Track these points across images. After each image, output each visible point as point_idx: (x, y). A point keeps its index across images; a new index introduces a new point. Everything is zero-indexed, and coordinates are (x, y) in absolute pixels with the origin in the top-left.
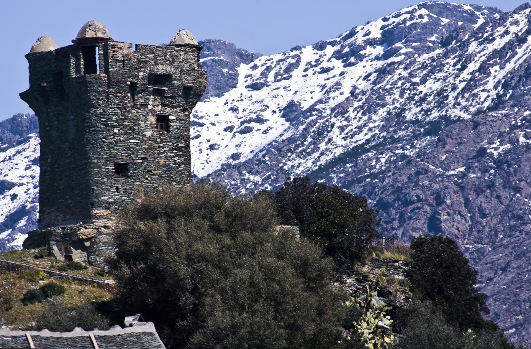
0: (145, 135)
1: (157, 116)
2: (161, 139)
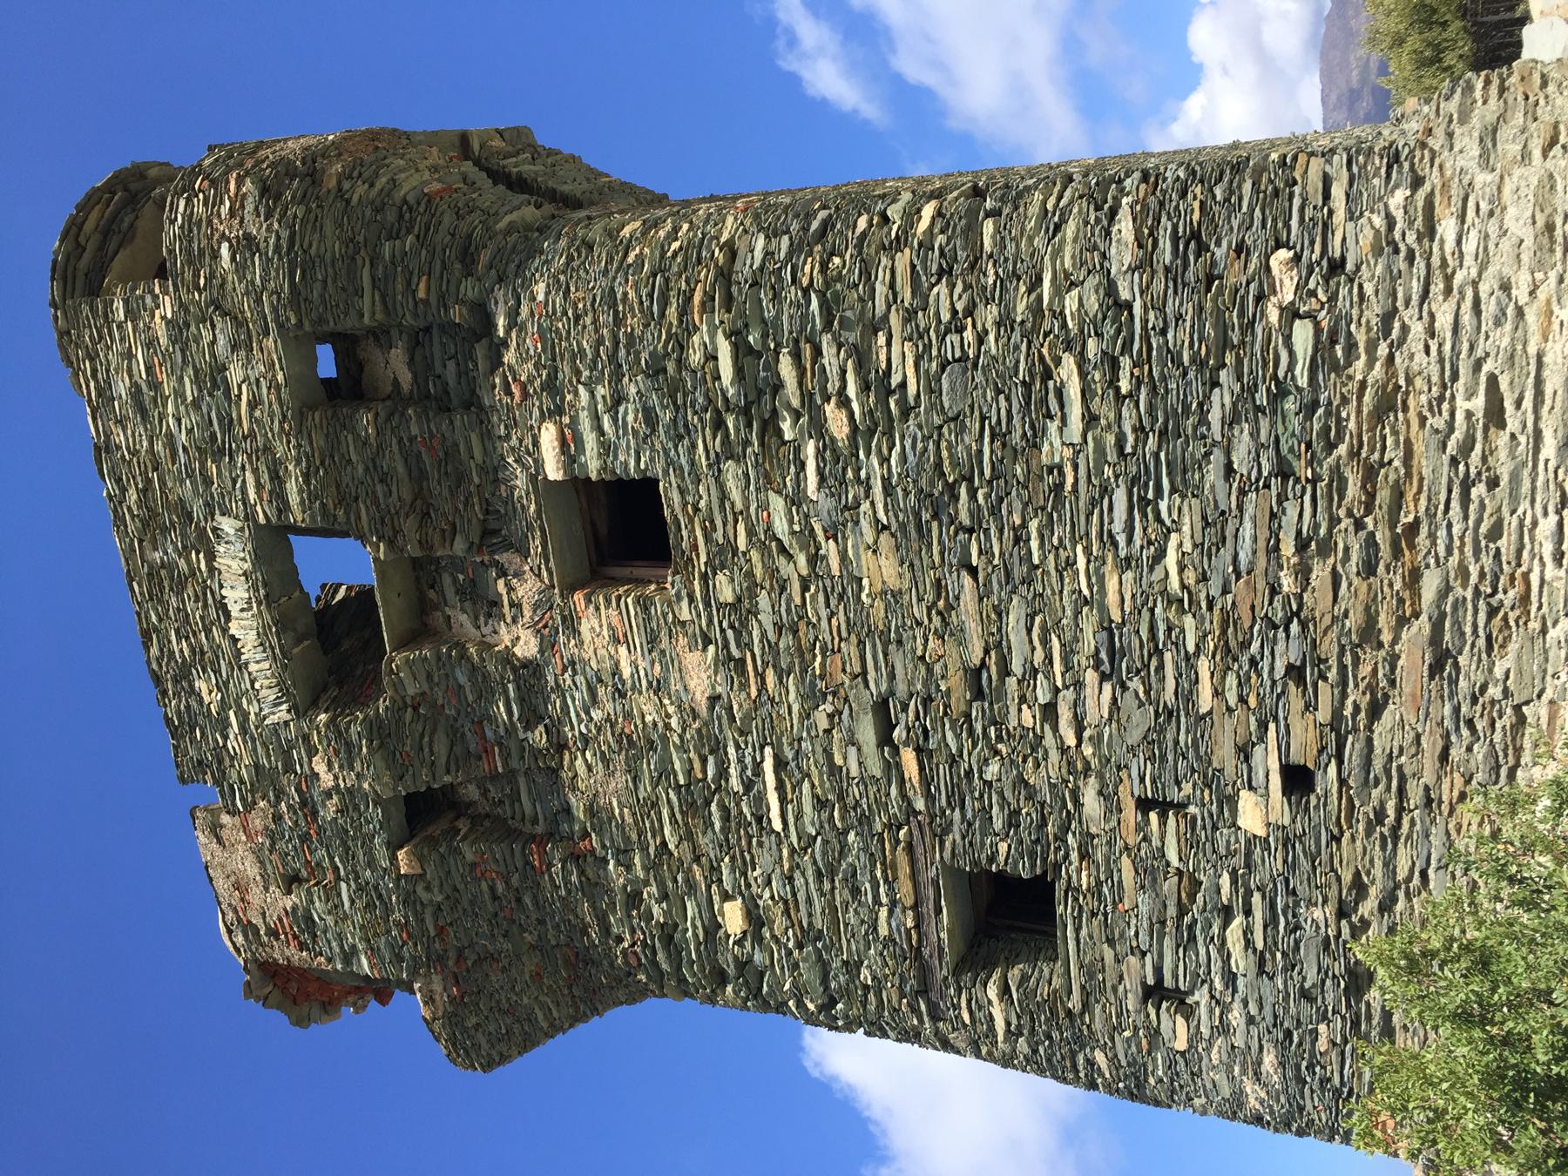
0: (714, 699)
1: (569, 589)
2: (714, 567)
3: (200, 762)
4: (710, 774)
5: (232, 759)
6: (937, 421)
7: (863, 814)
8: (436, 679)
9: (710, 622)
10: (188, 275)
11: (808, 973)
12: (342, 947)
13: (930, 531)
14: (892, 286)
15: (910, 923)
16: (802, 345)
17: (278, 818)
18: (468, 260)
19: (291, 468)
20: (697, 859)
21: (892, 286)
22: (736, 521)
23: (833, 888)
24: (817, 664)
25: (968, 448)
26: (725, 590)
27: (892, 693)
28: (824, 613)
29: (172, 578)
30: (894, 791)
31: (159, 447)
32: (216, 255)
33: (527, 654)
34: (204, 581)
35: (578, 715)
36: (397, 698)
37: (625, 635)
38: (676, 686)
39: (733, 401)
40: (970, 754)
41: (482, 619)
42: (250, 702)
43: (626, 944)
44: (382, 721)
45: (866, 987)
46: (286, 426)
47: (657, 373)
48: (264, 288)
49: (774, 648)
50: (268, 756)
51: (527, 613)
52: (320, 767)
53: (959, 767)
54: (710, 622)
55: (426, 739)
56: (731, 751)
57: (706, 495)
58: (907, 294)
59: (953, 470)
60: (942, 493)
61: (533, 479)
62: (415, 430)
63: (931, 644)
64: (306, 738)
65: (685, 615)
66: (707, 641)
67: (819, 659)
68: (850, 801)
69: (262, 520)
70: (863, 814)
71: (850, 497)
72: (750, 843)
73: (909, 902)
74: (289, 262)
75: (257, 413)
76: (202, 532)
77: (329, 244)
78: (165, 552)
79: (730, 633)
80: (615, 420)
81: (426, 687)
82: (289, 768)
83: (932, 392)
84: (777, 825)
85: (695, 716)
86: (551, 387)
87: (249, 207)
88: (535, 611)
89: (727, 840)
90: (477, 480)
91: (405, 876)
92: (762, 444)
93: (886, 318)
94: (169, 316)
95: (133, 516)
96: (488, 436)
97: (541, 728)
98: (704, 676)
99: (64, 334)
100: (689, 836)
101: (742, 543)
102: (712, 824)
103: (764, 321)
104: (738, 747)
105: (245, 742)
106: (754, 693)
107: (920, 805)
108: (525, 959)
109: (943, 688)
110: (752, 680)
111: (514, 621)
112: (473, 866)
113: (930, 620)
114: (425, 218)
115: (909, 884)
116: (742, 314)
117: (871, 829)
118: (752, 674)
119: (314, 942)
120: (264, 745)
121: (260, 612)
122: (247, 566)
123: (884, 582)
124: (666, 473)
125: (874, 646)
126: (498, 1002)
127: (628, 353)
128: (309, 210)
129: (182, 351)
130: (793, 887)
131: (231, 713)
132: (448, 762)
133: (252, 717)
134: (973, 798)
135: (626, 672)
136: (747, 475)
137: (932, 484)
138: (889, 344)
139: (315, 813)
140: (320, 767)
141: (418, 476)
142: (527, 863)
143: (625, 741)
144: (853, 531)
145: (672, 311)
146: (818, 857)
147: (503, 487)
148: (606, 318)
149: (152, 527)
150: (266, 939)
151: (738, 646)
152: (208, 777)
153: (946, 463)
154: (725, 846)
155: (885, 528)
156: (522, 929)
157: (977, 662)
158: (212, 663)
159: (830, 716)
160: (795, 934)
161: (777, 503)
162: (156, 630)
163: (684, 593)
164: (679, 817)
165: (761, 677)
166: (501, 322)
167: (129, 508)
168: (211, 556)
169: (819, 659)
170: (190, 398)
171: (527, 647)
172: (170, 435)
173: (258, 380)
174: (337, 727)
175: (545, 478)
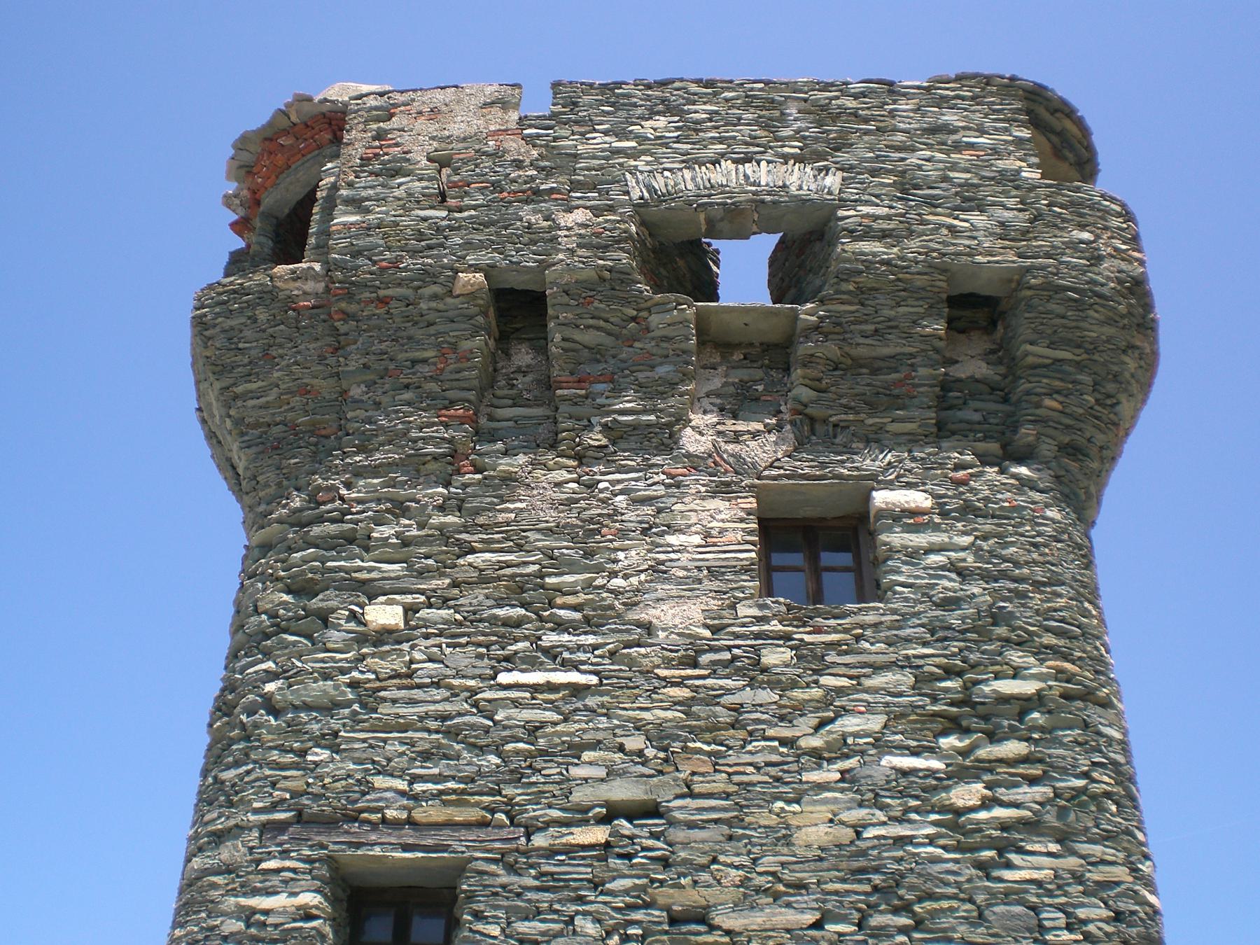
0: (648, 628)
3: (575, 104)
4: (562, 612)
5: (583, 134)
6: (980, 898)
7: (523, 775)
8: (664, 345)
9: (737, 636)
10: (1060, 199)
11: (318, 689)
12: (368, 199)
13: (860, 881)
14: (1103, 862)
15: (390, 813)
16: (1039, 766)
17: (518, 164)
18: (1070, 450)
19: (895, 250)
20: (455, 584)
21: (1103, 862)
22: (851, 677)
23: (429, 731)
24: (699, 745)
25: (954, 930)
26: (775, 657)
27: (672, 823)
28: (759, 759)
29: (771, 119)
30: (555, 813)
31: (900, 137)
32: (1082, 227)
33: (684, 441)
34: (771, 148)
35: (619, 482)
36: (649, 304)
37: (715, 545)
38: (662, 589)
39: (976, 689)
40: (605, 903)
41: (718, 401)
42: (648, 163)
43: (343, 492)
44: (628, 285)
45: (303, 753)
46: (935, 254)
47: (993, 616)
48: (1061, 263)
49: (713, 701)
50: (589, 169)
51: (730, 447)
52: (580, 216)
53: (589, 889)
54: (737, 636)
55: (602, 323)
56: (591, 639)
57: (874, 649)
58: (1095, 875)
59: (928, 912)
60: (901, 898)
61: (873, 477)
62: (922, 371)
63: (733, 872)
64: (611, 209)
65: (745, 611)
66: (715, 630)
67: (706, 748)
68: (539, 763)
69: (841, 213)
70: (523, 775)
71: (888, 800)
72: (479, 645)
73: (418, 815)
74: (1084, 290)
75: (945, 231)
76: (821, 156)
77: (1095, 328)
78: (795, 119)
79: (727, 656)
80: (943, 568)
81: (657, 333)
82: (576, 185)
83: (1006, 895)
84: (504, 678)
85: (630, 605)
86: (967, 510)
87: (1124, 266)
88: (732, 455)
89: (480, 621)
90: (870, 421)
91: (455, 277)
92: (935, 715)
93: (1074, 853)
94: (1024, 174)
95: (831, 99)
96: (911, 441)
97: (604, 442)
98: (677, 621)
99: (988, 80)
100: (483, 579)
101: (827, 680)
102: (500, 606)
103: (1054, 729)
104: (595, 647)
105: (603, 150)
106: (663, 672)
107: (539, 840)
108: (332, 381)
109: (683, 881)
110: (677, 673)
111: (719, 433)
112: (454, 347)
113: (760, 874)
114: (1104, 417)
115: (441, 819)
116: (1060, 708)
117: (505, 782)
118: (683, 673)
119: (371, 173)
120: (601, 168)
121: (747, 192)
122: (793, 189)
123: (799, 827)
124: (894, 612)
125: (725, 810)
126: (281, 346)
127: (1010, 590)
128: (1123, 316)
129: (993, 179)
130: (427, 686)
131: (633, 144)
132: (574, 341)
133: (633, 163)
134: (551, 903)
135: (672, 539)
136: (900, 695)
137: (911, 888)
138: (1050, 854)
139: (527, 202)
140: (580, 216)
141: (875, 367)
142: (452, 403)
143: (592, 528)
144: (852, 800)
145: (1049, 639)
146: (467, 719)
147: (861, 445)
148: (1040, 574)
149: (822, 114)
150: (375, 126)
151: (714, 663)
152: (559, 108)
153: (935, 905)
154: (473, 618)
155: (858, 834)
156: (370, 385)
157: (717, 921)
158: (687, 137)
159: (640, 753)
160: (369, 681)
161: (875, 723)
162: (715, 94)
163: (767, 613)
164: (508, 571)
165: (680, 683)
166: (1023, 470)
167: (837, 98)
168: (799, 159)
169: (706, 748)
170: (952, 174)
171: (692, 442)
172: (914, 150)
173: (975, 238)
174: (625, 240)
175: (874, 489)
